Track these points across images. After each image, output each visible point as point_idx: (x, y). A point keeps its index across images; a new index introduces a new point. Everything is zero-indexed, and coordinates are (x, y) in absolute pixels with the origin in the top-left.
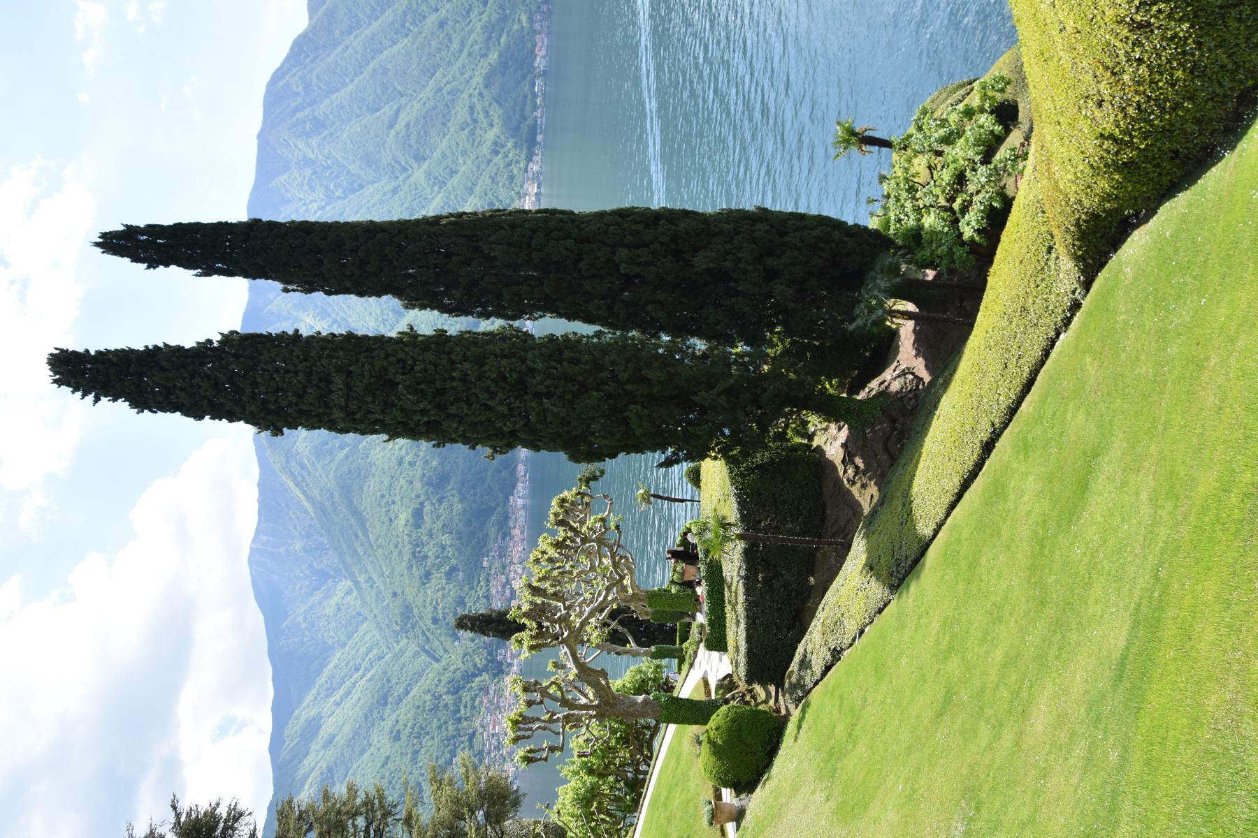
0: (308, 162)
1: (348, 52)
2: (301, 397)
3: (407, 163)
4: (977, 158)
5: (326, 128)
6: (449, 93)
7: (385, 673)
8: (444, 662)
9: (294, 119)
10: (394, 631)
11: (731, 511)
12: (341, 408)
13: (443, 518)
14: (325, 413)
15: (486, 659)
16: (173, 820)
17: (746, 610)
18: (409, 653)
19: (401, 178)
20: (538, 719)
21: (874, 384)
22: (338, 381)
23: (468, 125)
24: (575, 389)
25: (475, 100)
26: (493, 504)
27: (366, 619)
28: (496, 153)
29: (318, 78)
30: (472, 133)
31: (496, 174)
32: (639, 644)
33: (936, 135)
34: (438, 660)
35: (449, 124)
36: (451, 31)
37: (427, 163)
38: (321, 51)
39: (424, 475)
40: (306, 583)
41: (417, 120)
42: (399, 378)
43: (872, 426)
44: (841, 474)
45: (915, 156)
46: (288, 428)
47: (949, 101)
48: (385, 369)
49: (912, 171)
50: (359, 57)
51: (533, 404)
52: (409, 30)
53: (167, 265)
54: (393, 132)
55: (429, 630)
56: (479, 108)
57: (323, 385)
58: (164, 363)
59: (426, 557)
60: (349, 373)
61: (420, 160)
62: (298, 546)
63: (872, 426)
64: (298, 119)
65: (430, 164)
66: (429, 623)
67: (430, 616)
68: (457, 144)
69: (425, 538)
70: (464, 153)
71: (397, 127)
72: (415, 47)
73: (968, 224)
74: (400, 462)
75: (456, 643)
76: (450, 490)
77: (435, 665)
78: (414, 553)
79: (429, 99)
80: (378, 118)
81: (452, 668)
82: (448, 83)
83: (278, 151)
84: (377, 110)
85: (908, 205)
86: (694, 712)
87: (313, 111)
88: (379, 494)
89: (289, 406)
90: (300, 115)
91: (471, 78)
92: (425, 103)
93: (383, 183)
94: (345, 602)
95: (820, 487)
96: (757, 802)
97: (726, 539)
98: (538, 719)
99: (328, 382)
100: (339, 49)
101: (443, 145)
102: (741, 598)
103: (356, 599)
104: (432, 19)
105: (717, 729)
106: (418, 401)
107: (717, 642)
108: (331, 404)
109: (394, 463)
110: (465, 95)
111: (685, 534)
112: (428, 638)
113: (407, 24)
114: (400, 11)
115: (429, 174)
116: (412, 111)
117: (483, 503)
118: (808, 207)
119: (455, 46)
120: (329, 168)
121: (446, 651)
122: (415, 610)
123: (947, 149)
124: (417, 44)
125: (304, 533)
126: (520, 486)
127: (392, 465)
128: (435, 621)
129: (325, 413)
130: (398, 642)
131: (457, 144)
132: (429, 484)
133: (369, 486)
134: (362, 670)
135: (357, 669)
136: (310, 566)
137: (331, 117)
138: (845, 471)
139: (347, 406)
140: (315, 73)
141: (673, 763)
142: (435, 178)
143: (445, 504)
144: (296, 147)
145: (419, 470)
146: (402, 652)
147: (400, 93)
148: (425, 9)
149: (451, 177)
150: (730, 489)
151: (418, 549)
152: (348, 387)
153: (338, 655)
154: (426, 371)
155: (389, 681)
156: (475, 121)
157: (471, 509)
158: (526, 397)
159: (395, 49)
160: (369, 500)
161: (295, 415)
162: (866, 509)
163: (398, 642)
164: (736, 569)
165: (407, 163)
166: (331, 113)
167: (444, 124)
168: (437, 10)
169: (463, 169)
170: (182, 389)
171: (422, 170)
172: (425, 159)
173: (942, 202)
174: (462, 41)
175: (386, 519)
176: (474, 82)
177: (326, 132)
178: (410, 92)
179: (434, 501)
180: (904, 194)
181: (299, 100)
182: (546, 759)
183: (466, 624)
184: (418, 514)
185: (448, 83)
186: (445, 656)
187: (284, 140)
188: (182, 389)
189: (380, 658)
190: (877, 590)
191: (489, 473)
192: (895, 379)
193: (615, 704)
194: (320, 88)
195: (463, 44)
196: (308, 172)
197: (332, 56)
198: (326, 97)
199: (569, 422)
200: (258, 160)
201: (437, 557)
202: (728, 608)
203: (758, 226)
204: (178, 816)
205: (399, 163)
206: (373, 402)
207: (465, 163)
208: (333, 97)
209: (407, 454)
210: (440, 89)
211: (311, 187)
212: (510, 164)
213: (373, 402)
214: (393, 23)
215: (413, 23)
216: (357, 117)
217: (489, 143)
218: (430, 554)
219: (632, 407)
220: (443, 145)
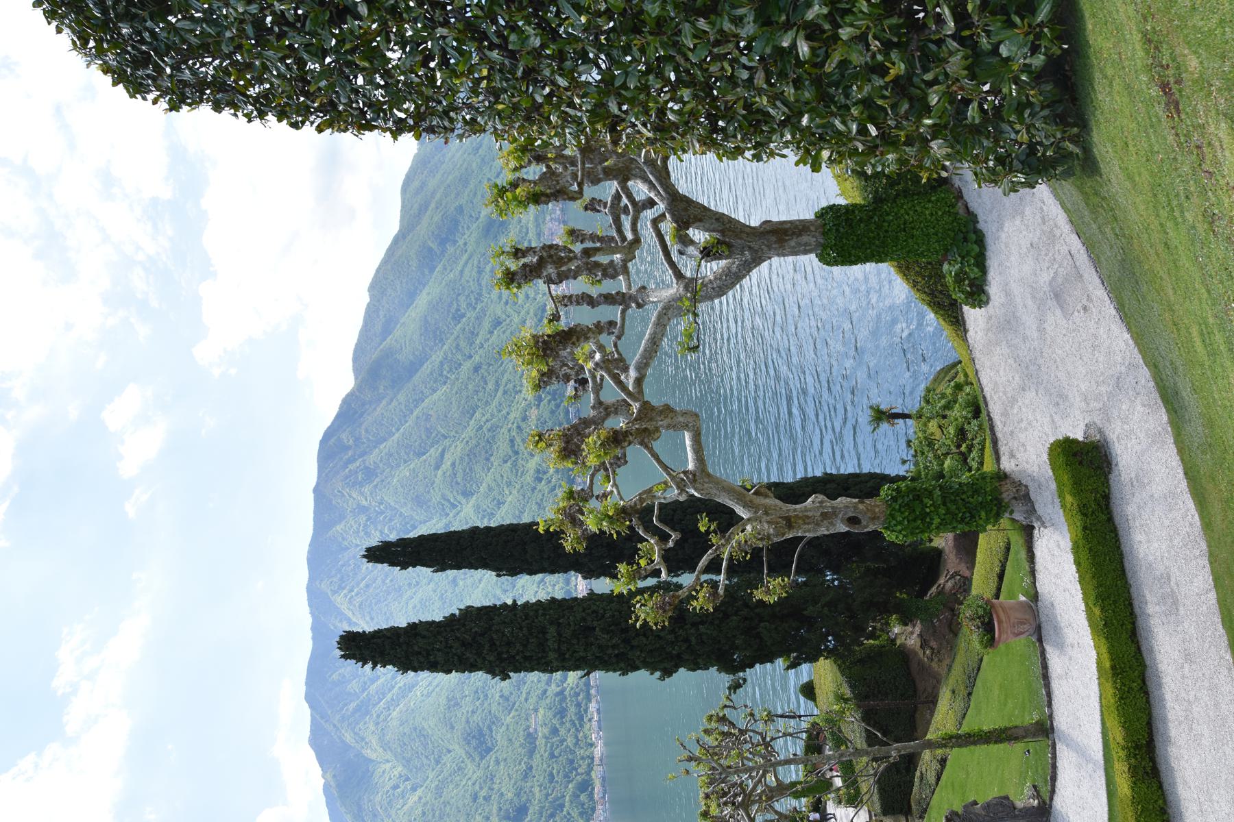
0: (363, 509)
1: (393, 404)
2: (525, 646)
3: (455, 499)
4: (970, 416)
5: (377, 476)
6: (489, 430)
9: (347, 470)
12: (555, 650)
14: (542, 657)
19: (451, 515)
21: (934, 590)
22: (552, 631)
23: (510, 457)
24: (721, 616)
25: (514, 433)
28: (540, 480)
29: (367, 431)
30: (515, 464)
31: (542, 500)
33: (940, 405)
35: (492, 459)
36: (486, 374)
37: (474, 498)
38: (367, 407)
39: (500, 809)
41: (461, 459)
42: (595, 623)
43: (937, 616)
44: (921, 656)
45: (929, 421)
46: (515, 672)
47: (947, 378)
48: (584, 619)
49: (929, 432)
50: (403, 407)
51: (693, 631)
52: (447, 378)
53: (414, 566)
54: (440, 472)
56: (518, 440)
57: (541, 635)
58: (425, 633)
60: (559, 624)
61: (468, 495)
63: (937, 616)
64: (350, 470)
65: (477, 500)
68: (502, 476)
70: (509, 484)
71: (444, 467)
72: (454, 392)
73: (973, 459)
74: (475, 798)
79: (471, 438)
80: (425, 461)
82: (487, 421)
83: (334, 502)
84: (424, 454)
85: (931, 455)
87: (364, 461)
89: (518, 654)
90: (351, 467)
91: (508, 414)
92: (468, 442)
93: (434, 521)
95: (908, 669)
99: (544, 632)
100: (384, 402)
101: (489, 478)
104: (467, 366)
106: (611, 638)
108: (547, 649)
110: (504, 430)
113: (445, 373)
114: (437, 362)
115: (477, 508)
116: (456, 451)
118: (859, 465)
119: (491, 386)
120: (382, 513)
123: (948, 413)
124: (456, 389)
127: (466, 802)
129: (542, 657)
131: (502, 476)
137: (381, 465)
138: (924, 653)
139: (559, 648)
140: (363, 427)
142: (484, 511)
144: (350, 496)
145: (495, 804)
147: (443, 435)
148: (460, 357)
149: (499, 508)
152: (560, 635)
154: (613, 616)
156: (517, 453)
158: (686, 627)
159: (435, 396)
161: (522, 660)
165: (455, 499)
166: (381, 461)
167: (487, 459)
168: (470, 357)
169: (509, 499)
170: (439, 650)
171: (470, 504)
172: (473, 494)
173: (954, 450)
174: (497, 382)
176: (511, 417)
177: (378, 480)
178: (453, 433)
180: (926, 449)
181: (350, 453)
185: (487, 421)
187: (339, 491)
188: (439, 650)
191: (567, 798)
192: (947, 581)
194: (369, 440)
195: (497, 384)
196: (363, 519)
197: (378, 409)
198: (375, 447)
199: (719, 641)
200: (315, 513)
203: (828, 486)
205: (449, 501)
206: (578, 644)
207: (511, 493)
208: (382, 447)
209: (481, 788)
210: (481, 428)
211: (366, 533)
212: (554, 489)
213: (578, 644)
214: (431, 374)
215: (450, 371)
216: (405, 462)
217: (532, 472)
219: (762, 624)
220: (489, 478)
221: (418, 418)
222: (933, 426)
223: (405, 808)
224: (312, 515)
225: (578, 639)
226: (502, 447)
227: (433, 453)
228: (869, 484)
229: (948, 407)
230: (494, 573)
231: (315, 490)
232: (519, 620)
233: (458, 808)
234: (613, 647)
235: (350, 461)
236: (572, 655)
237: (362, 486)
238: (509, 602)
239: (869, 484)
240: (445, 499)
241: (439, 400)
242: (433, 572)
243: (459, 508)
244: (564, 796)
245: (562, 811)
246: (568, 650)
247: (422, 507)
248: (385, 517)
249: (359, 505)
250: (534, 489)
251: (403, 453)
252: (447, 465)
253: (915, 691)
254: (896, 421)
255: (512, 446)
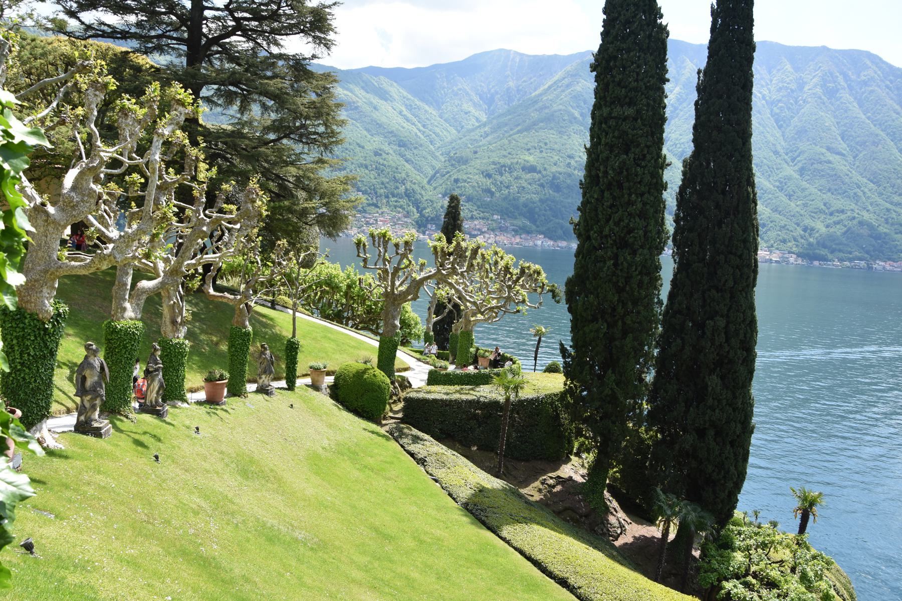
2: (619, 84)
3: (799, 161)
7: (421, 145)
8: (427, 186)
9: (838, 74)
10: (450, 152)
11: (526, 393)
12: (610, 113)
13: (529, 187)
15: (429, 216)
16: (327, 4)
17: (456, 400)
18: (434, 162)
19: (786, 157)
20: (386, 251)
21: (615, 504)
22: (630, 111)
23: (828, 209)
24: (620, 284)
25: (849, 214)
26: (538, 223)
27: (459, 132)
28: (805, 230)
29: (872, 91)
30: (822, 211)
31: (788, 230)
32: (435, 324)
33: (808, 569)
34: (429, 182)
35: (829, 194)
37: (798, 177)
40: (485, 90)
41: (833, 169)
42: (631, 156)
43: (584, 500)
44: (550, 475)
45: (791, 551)
49: (779, 547)
50: (889, 123)
54: (824, 150)
55: (450, 176)
56: (843, 217)
57: (627, 100)
59: (501, 174)
60: (635, 119)
62: (511, 84)
64: (837, 77)
66: (455, 177)
67: (460, 177)
68: (813, 200)
69: (515, 174)
71: (828, 154)
73: (735, 586)
74: (570, 157)
75: (440, 196)
76: (549, 192)
77: (425, 181)
78: (504, 166)
80: (836, 139)
81: (423, 192)
82: (864, 193)
84: (843, 139)
85: (752, 542)
86: (386, 360)
87: (844, 88)
88: (547, 141)
89: (612, 76)
91: (868, 211)
93: (783, 143)
94: (471, 117)
96: (324, 400)
97: (507, 388)
98: (386, 251)
102: (464, 397)
103: (473, 125)
105: (374, 375)
106: (614, 170)
107: (434, 379)
108: (613, 106)
109: (569, 152)
110: (853, 206)
111: (511, 360)
112: (444, 175)
115: (790, 178)
116: (840, 165)
117: (539, 216)
120: (796, 102)
121: (435, 188)
122: (464, 167)
123: (796, 577)
125: (521, 88)
126: (551, 243)
128: (456, 181)
129: (606, 101)
130: (442, 154)
131: (813, 200)
132: (554, 177)
133: (553, 134)
134: (424, 130)
135: (424, 126)
136: (497, 93)
137: (838, 103)
138: (551, 478)
139: (612, 118)
141: (353, 343)
142: (786, 184)
143: (539, 189)
144: (814, 76)
146: (435, 157)
147: (857, 155)
149: (786, 195)
150: (542, 394)
151: (507, 169)
152: (625, 119)
153: (434, 113)
155: (416, 148)
156: (831, 214)
157: (535, 207)
158: (615, 248)
160: (543, 134)
161: (605, 80)
162: (523, 491)
163: (442, 154)
164: (485, 395)
165: (799, 161)
166: (842, 103)
167: (829, 190)
171: (793, 173)
173: (753, 568)
175: (529, 146)
176: (865, 213)
178: (857, 163)
179: (542, 181)
180: (760, 539)
181: (854, 77)
182: (358, 256)
183: (453, 202)
184: (532, 169)
185: (864, 193)
186: (432, 188)
187: (820, 67)
189: (431, 142)
190: (465, 493)
191: (561, 221)
193: (394, 305)
194: (863, 93)
197: (891, 102)
199: (595, 279)
201: (501, 183)
202: (457, 387)
203: (739, 425)
204: (329, 7)
205: (798, 156)
206: (613, 137)
207: (797, 206)
208: (855, 104)
210: (859, 187)
211: (781, 88)
212: (795, 240)
216: (838, 123)
217: (813, 224)
218: (504, 177)
221: (877, 135)
222: (785, 554)
223: (570, 108)
224: (802, 45)
225: (619, 137)
226: (838, 203)
227: (843, 146)
228: (732, 469)
229: (804, 578)
230: (702, 68)
231: (824, 48)
232: (646, 80)
233: (565, 144)
234: (606, 173)
235: (845, 76)
236: (604, 130)
237: (822, 87)
238: (667, 76)
239: (732, 469)
240: (800, 153)
241: (891, 154)
242: (712, 4)
243: (791, 164)
244: (563, 219)
245: (553, 216)
246: (610, 127)
247: (796, 134)
248: (791, 104)
249: (805, 83)
250: (798, 225)
251: (846, 121)
252: (830, 156)
253: (518, 459)
254: (799, 516)
255: (838, 211)
